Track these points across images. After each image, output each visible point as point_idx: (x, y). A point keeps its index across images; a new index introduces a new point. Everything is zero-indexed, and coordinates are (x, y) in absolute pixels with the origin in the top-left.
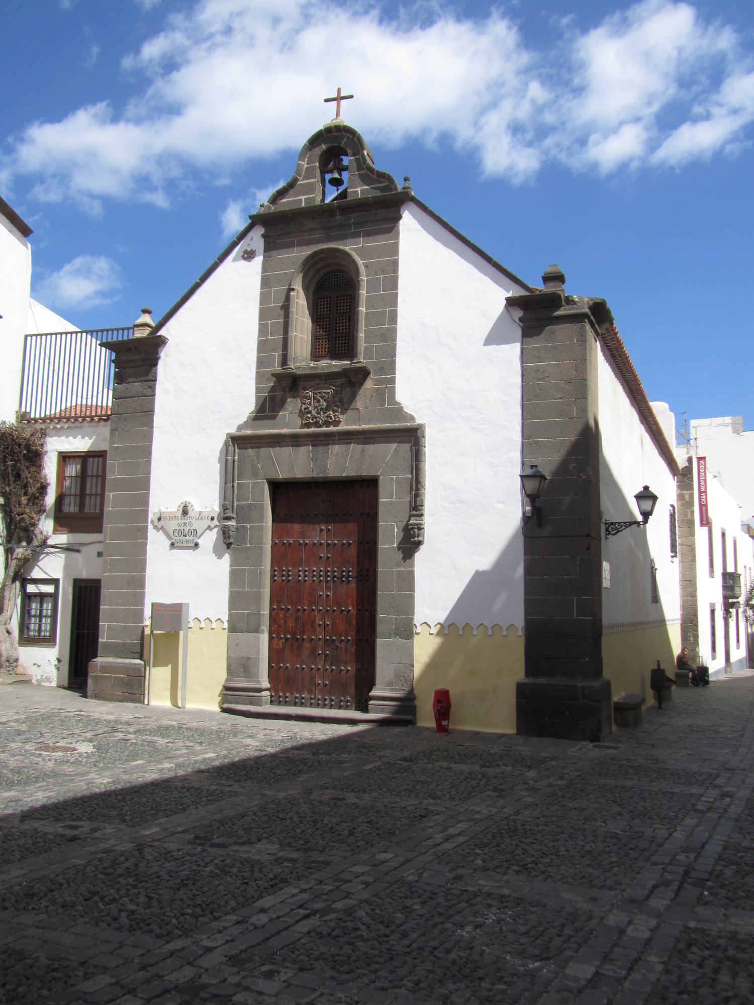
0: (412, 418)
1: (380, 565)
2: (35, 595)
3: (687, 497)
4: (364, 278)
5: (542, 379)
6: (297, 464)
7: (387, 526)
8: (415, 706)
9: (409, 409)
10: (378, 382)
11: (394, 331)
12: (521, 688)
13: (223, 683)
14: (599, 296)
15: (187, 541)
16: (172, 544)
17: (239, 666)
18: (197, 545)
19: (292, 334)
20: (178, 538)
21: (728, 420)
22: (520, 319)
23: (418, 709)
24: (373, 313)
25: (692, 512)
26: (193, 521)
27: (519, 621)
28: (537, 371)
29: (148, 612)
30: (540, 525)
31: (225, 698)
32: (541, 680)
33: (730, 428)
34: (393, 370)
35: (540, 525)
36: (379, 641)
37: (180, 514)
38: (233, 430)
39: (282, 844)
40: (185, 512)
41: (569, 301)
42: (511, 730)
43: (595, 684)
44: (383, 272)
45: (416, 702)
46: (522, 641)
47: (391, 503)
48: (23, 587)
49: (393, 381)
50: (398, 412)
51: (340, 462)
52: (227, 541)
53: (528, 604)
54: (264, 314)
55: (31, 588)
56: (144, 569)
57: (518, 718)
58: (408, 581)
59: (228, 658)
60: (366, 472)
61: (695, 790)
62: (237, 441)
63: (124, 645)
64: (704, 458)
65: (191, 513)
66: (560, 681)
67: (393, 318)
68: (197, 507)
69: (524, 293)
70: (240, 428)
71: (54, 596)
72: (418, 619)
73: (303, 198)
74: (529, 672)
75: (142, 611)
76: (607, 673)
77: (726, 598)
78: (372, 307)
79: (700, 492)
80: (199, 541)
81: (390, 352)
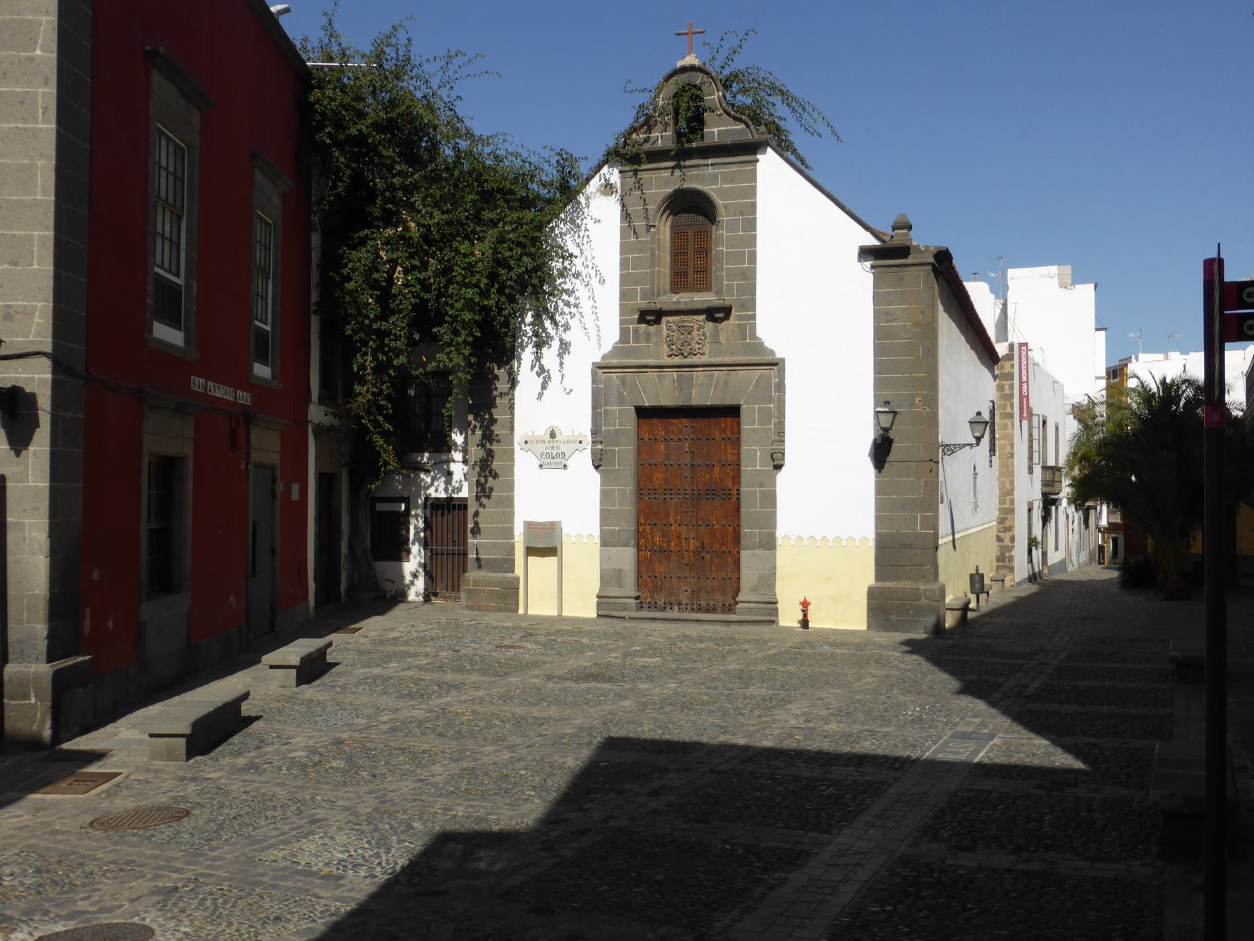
0: (773, 353)
1: (51, 274)
3: (1007, 387)
5: (892, 321)
6: (663, 393)
7: (749, 451)
9: (768, 344)
10: (740, 318)
11: (754, 271)
12: (872, 593)
13: (597, 591)
14: (943, 244)
17: (608, 577)
21: (1054, 269)
25: (1012, 405)
27: (871, 534)
28: (887, 313)
29: (519, 529)
31: (599, 605)
32: (889, 584)
33: (1056, 280)
34: (753, 308)
36: (743, 553)
37: (547, 438)
38: (598, 360)
39: (768, 688)
40: (553, 435)
41: (917, 248)
42: (862, 626)
43: (935, 587)
44: (742, 213)
46: (872, 552)
47: (754, 430)
48: (373, 507)
49: (753, 317)
50: (759, 346)
51: (704, 392)
53: (879, 519)
56: (512, 489)
57: (868, 617)
58: (770, 499)
59: (602, 570)
60: (729, 401)
61: (1020, 662)
62: (598, 367)
63: (495, 560)
64: (1026, 344)
65: (558, 437)
66: (905, 584)
67: (753, 258)
68: (564, 432)
69: (877, 243)
70: (604, 357)
72: (780, 534)
74: (878, 577)
76: (942, 578)
77: (1044, 495)
78: (732, 247)
80: (568, 463)
81: (751, 290)
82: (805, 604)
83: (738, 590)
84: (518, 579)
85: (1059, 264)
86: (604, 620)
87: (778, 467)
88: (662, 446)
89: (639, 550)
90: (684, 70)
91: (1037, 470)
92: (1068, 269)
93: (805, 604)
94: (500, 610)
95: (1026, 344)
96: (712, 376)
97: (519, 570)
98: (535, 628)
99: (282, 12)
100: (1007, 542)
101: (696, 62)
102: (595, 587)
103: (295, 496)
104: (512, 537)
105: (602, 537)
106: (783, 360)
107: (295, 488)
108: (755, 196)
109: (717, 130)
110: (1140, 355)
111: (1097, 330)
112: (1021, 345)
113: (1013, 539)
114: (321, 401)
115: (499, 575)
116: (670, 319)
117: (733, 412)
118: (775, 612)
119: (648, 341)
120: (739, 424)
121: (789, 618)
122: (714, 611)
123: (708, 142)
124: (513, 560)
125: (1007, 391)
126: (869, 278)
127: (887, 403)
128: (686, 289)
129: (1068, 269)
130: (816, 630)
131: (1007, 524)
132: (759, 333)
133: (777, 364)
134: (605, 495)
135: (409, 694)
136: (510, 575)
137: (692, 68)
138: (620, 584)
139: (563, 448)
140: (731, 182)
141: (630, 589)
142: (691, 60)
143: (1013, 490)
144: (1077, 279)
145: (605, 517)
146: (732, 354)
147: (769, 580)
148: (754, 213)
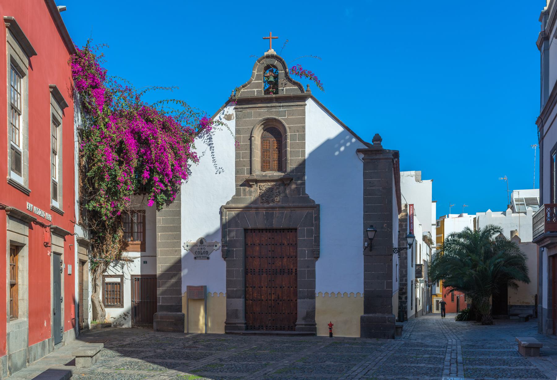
0: (314, 201)
2: (110, 283)
4: (289, 134)
8: (316, 328)
12: (362, 319)
15: (203, 257)
16: (195, 258)
17: (231, 314)
18: (208, 258)
19: (253, 159)
20: (198, 255)
21: (413, 173)
22: (363, 159)
23: (317, 329)
24: (294, 151)
26: (206, 247)
27: (362, 292)
29: (184, 290)
30: (371, 250)
31: (226, 328)
32: (371, 315)
35: (371, 250)
36: (299, 300)
44: (298, 131)
45: (316, 326)
47: (304, 240)
48: (104, 280)
50: (306, 199)
52: (226, 255)
54: (238, 146)
55: (108, 280)
58: (312, 274)
63: (172, 306)
64: (413, 205)
65: (205, 243)
70: (228, 203)
71: (120, 285)
72: (317, 291)
73: (256, 90)
74: (365, 312)
75: (180, 290)
79: (410, 223)
82: (331, 325)
83: (296, 319)
84: (184, 315)
85: (416, 170)
86: (228, 335)
87: (317, 258)
88: (258, 248)
89: (246, 300)
90: (268, 57)
91: (414, 266)
92: (419, 173)
93: (331, 325)
94: (174, 331)
95: (413, 205)
96: (283, 213)
97: (184, 311)
98: (197, 338)
99: (63, 10)
100: (403, 299)
101: (275, 53)
102: (224, 318)
103: (70, 272)
104: (181, 294)
105: (227, 293)
106: (319, 205)
107: (70, 267)
108: (305, 123)
109: (286, 89)
110: (450, 215)
111: (433, 202)
112: (410, 205)
113: (406, 298)
114: (80, 224)
115: (174, 313)
116: (262, 184)
117: (296, 229)
118: (315, 329)
119: (250, 195)
120: (296, 237)
121: (322, 332)
122: (284, 329)
123: (280, 94)
124: (181, 305)
125: (404, 227)
126: (361, 165)
127: (372, 226)
128: (11, 245)
129: (419, 173)
130: (336, 337)
131: (404, 291)
132: (307, 192)
133: (317, 207)
134: (229, 273)
135: (153, 369)
136: (180, 313)
137: (272, 56)
138: (237, 317)
139: (207, 249)
140: (292, 115)
141: (241, 320)
142: (272, 52)
143: (407, 274)
144: (424, 178)
145: (229, 283)
146: (293, 202)
147: (311, 315)
148: (304, 131)
